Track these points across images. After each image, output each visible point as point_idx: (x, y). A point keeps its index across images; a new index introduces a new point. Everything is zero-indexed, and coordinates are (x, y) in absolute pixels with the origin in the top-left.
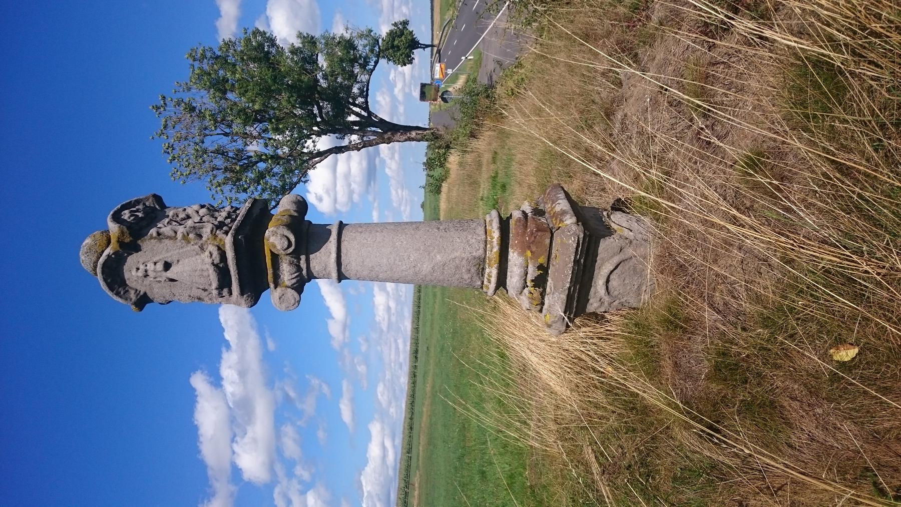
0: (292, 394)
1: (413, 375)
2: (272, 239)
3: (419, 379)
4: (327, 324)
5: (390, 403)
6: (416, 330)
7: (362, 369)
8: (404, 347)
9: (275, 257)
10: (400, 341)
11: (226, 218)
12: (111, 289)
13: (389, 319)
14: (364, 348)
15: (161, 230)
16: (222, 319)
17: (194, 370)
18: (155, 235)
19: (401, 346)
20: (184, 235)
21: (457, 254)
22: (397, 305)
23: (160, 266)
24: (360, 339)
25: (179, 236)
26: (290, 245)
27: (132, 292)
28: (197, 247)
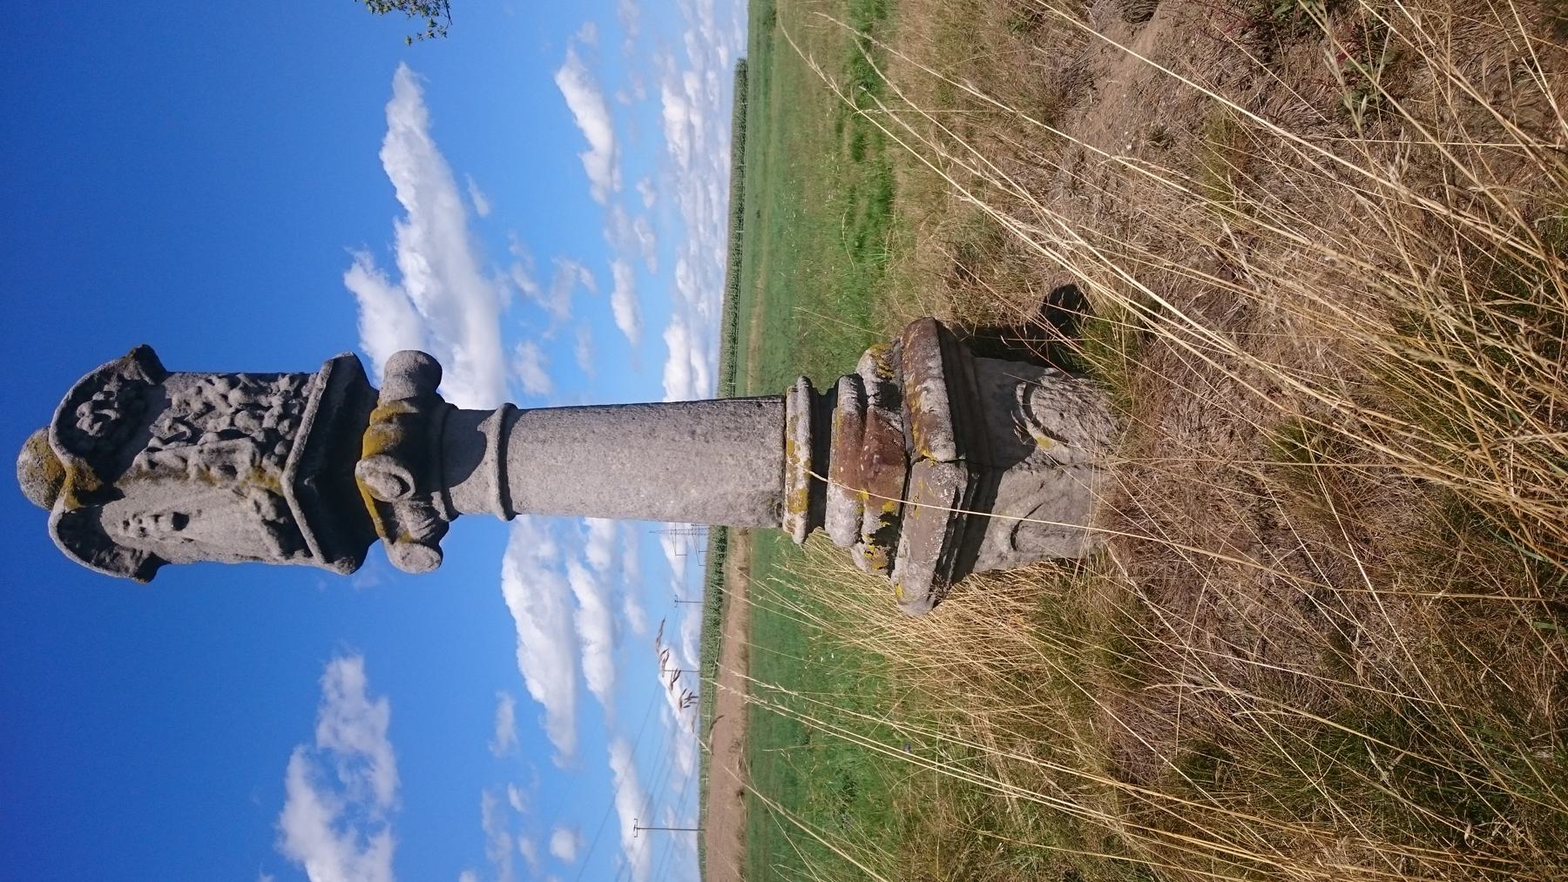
0: (528, 287)
1: (736, 252)
2: (370, 481)
3: (746, 260)
4: (581, 164)
5: (698, 292)
6: (739, 170)
7: (646, 240)
8: (719, 199)
9: (385, 509)
10: (712, 188)
11: (281, 418)
12: (87, 559)
13: (692, 146)
14: (649, 201)
15: (157, 456)
16: (388, 168)
17: (348, 263)
18: (145, 467)
19: (714, 196)
20: (200, 470)
21: (730, 488)
22: (705, 119)
23: (166, 524)
24: (641, 188)
25: (192, 471)
26: (405, 487)
27: (127, 555)
28: (228, 491)
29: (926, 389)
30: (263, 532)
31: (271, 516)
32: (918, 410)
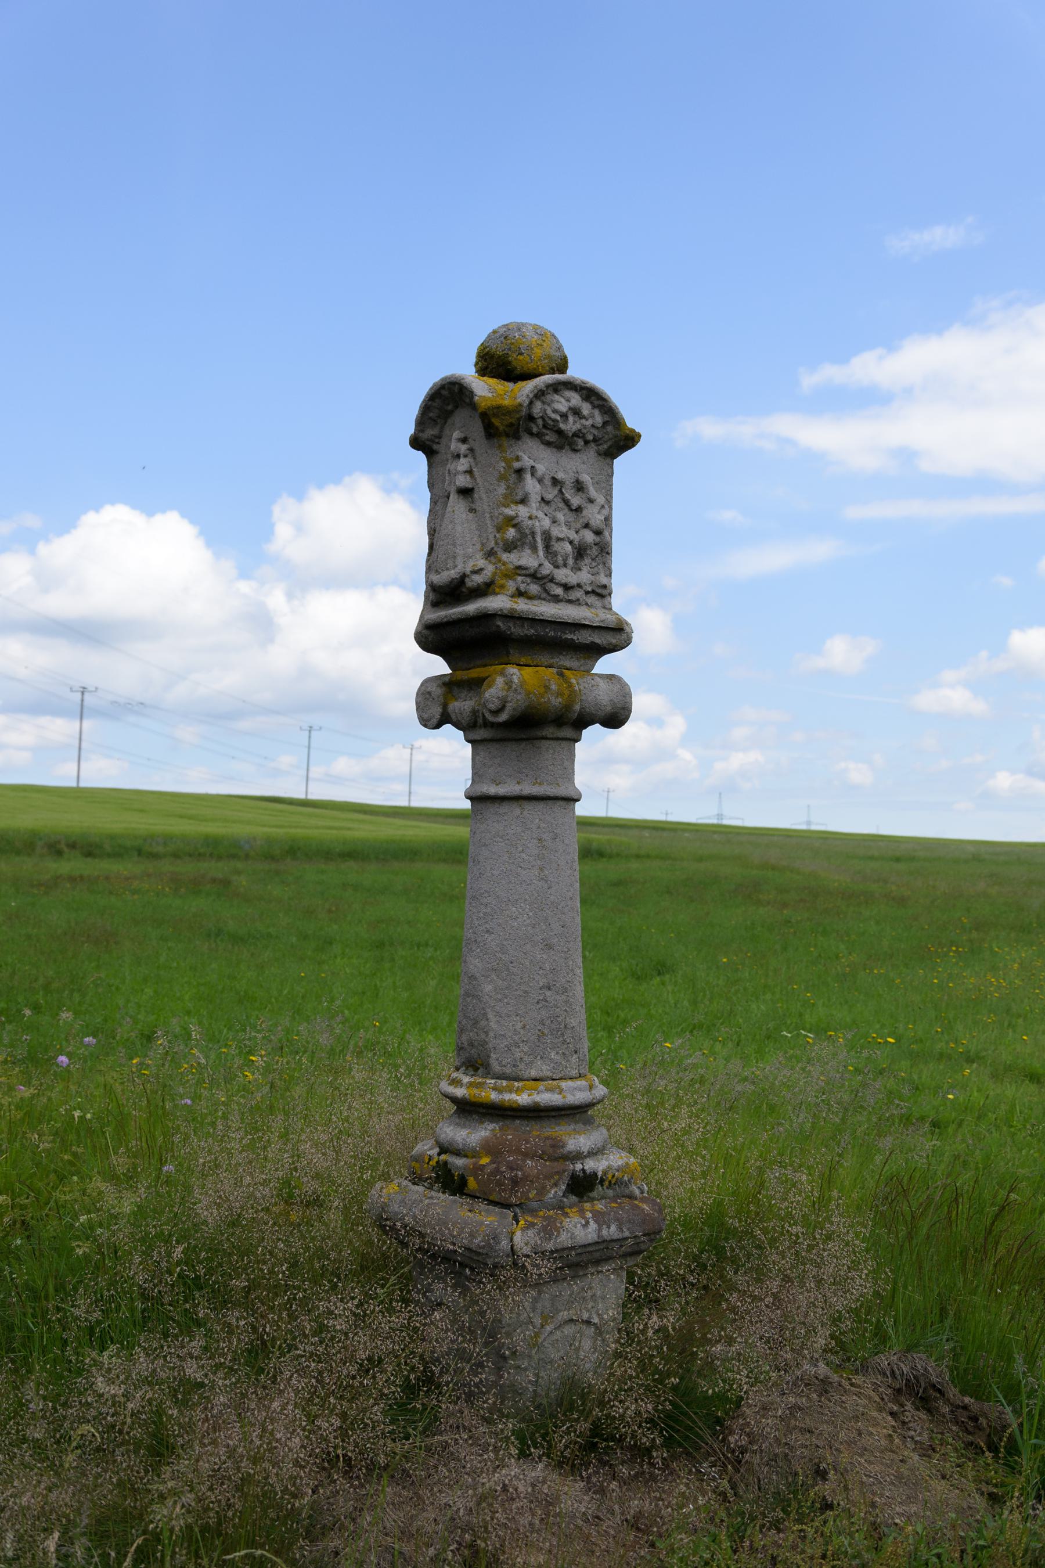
2: (500, 681)
9: (476, 685)
23: (462, 481)
26: (497, 712)
28: (492, 544)
29: (587, 1223)
30: (453, 573)
31: (469, 583)
32: (566, 1215)
